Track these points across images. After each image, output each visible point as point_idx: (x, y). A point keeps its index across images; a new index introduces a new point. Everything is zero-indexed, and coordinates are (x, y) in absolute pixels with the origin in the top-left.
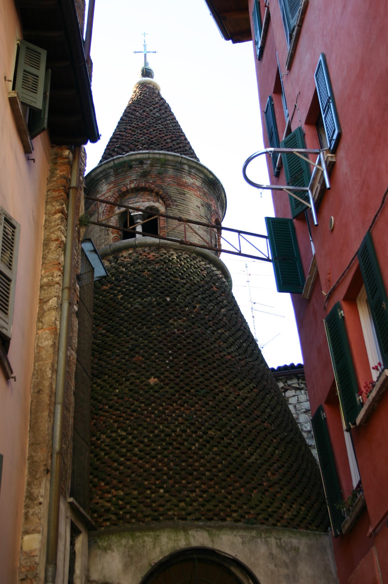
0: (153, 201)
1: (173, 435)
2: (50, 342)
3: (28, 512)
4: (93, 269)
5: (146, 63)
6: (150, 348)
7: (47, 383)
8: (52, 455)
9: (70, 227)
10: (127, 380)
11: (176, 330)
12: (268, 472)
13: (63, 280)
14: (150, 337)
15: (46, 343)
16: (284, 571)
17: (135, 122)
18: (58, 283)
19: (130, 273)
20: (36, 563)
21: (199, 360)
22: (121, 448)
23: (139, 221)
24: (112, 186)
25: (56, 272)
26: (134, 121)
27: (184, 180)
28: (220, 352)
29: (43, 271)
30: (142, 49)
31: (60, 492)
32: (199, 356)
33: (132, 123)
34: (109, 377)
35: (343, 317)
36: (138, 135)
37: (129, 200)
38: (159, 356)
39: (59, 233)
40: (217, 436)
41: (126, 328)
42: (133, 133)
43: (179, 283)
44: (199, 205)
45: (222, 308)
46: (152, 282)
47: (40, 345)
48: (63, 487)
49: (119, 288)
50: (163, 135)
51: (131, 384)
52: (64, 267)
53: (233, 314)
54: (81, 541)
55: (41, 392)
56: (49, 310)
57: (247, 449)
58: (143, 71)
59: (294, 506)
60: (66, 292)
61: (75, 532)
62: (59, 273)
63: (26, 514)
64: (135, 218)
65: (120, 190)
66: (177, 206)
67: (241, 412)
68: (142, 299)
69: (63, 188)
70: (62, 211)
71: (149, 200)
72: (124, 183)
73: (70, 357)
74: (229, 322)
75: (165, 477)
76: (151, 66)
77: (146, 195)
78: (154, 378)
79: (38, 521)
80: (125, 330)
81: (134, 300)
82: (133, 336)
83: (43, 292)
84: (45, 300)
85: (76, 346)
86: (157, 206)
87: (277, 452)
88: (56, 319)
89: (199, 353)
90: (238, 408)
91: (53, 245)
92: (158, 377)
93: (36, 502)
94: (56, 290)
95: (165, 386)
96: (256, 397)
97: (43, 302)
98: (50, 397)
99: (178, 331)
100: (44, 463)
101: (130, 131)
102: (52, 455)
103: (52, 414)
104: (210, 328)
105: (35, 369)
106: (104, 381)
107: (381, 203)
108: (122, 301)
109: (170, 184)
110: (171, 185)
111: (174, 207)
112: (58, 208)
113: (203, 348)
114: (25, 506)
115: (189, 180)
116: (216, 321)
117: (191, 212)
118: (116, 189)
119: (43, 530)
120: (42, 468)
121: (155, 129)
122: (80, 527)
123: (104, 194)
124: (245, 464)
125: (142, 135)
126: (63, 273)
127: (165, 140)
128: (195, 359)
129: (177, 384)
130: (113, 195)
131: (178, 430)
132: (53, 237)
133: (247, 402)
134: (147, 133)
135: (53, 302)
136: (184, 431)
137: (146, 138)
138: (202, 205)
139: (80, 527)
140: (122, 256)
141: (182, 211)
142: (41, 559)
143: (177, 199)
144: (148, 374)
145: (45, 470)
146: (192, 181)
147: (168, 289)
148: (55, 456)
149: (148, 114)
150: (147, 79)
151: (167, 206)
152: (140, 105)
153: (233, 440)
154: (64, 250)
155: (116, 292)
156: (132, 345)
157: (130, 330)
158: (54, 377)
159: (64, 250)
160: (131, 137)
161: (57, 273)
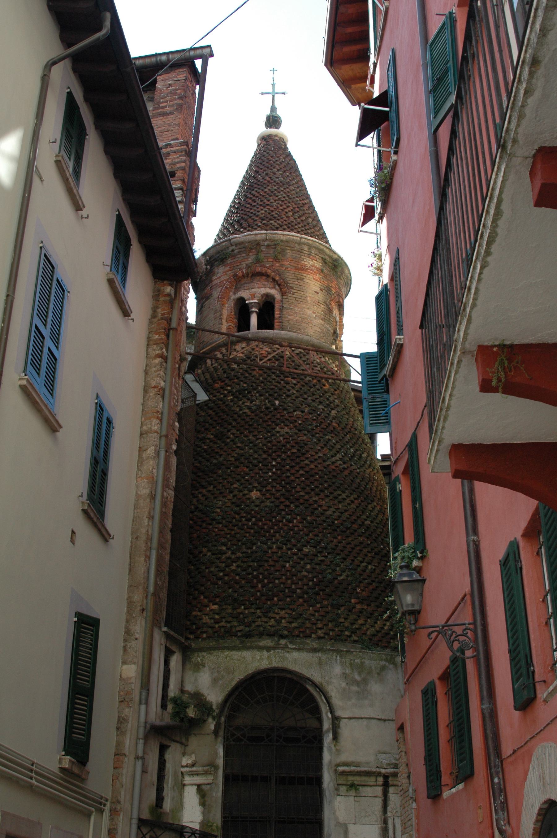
0: (269, 288)
1: (270, 552)
2: (147, 491)
3: (126, 645)
4: (196, 394)
5: (273, 109)
6: (255, 459)
7: (144, 531)
8: (147, 596)
9: (169, 372)
10: (231, 492)
11: (281, 438)
12: (357, 588)
13: (161, 427)
14: (256, 446)
15: (144, 491)
16: (355, 688)
17: (256, 190)
18: (156, 432)
19: (241, 371)
20: (132, 689)
21: (301, 472)
22: (220, 562)
23: (253, 309)
24: (227, 268)
25: (155, 420)
26: (256, 188)
27: (303, 262)
28: (324, 461)
29: (143, 419)
30: (270, 90)
31: (155, 623)
32: (302, 468)
33: (253, 190)
34: (214, 487)
35: (401, 491)
36: (258, 206)
37: (246, 285)
38: (263, 467)
39: (158, 379)
40: (311, 553)
41: (233, 434)
42: (254, 204)
43: (289, 383)
44: (318, 290)
45: (332, 409)
46: (262, 382)
47: (139, 493)
48: (158, 619)
49: (229, 388)
50: (285, 207)
51: (234, 496)
52: (162, 413)
53: (344, 414)
54: (175, 660)
55: (139, 539)
56: (147, 458)
57: (340, 566)
58: (268, 118)
59: (379, 622)
60: (163, 439)
61: (168, 653)
62: (158, 421)
63: (125, 647)
64: (250, 306)
65: (235, 275)
66: (293, 293)
67: (338, 527)
68: (251, 402)
69: (163, 330)
70: (161, 356)
71: (265, 286)
72: (240, 267)
73: (167, 498)
74: (338, 425)
75: (258, 594)
76: (279, 112)
77: (262, 280)
78: (257, 491)
79: (134, 654)
80: (232, 436)
81: (243, 403)
82: (239, 445)
83: (142, 439)
84: (144, 448)
85: (174, 484)
86: (273, 293)
87: (370, 567)
88: (153, 468)
89: (302, 464)
90: (336, 522)
91: (152, 392)
92: (260, 491)
93: (133, 637)
94: (153, 438)
95: (265, 500)
96: (356, 510)
97: (141, 450)
98: (147, 543)
99: (284, 439)
100: (140, 604)
101: (250, 201)
102: (147, 596)
103: (148, 557)
104: (317, 435)
105: (134, 517)
106: (209, 491)
107: (420, 416)
108: (232, 404)
109: (288, 268)
110: (289, 269)
111: (290, 295)
112: (157, 352)
113: (307, 458)
114: (124, 640)
115: (309, 262)
116: (323, 426)
117: (309, 299)
118: (230, 273)
119: (138, 662)
120: (139, 608)
121: (277, 198)
122: (174, 648)
123: (219, 278)
124: (336, 581)
125: (262, 208)
126: (161, 420)
127: (286, 213)
128: (298, 471)
129: (277, 499)
130: (228, 279)
131: (274, 546)
132: (153, 384)
133: (346, 515)
134: (268, 205)
135: (151, 451)
136: (280, 548)
137: (266, 211)
138: (321, 290)
139: (174, 648)
140: (235, 350)
141: (298, 299)
142: (136, 687)
143: (295, 286)
144: (251, 486)
145: (140, 610)
146: (311, 263)
147: (278, 391)
148: (149, 597)
149: (270, 178)
150: (273, 131)
151: (283, 294)
152: (264, 165)
153: (326, 557)
154: (163, 397)
155: (226, 392)
156: (238, 454)
157: (237, 437)
158: (151, 524)
159: (163, 397)
160: (251, 209)
161: (155, 421)
